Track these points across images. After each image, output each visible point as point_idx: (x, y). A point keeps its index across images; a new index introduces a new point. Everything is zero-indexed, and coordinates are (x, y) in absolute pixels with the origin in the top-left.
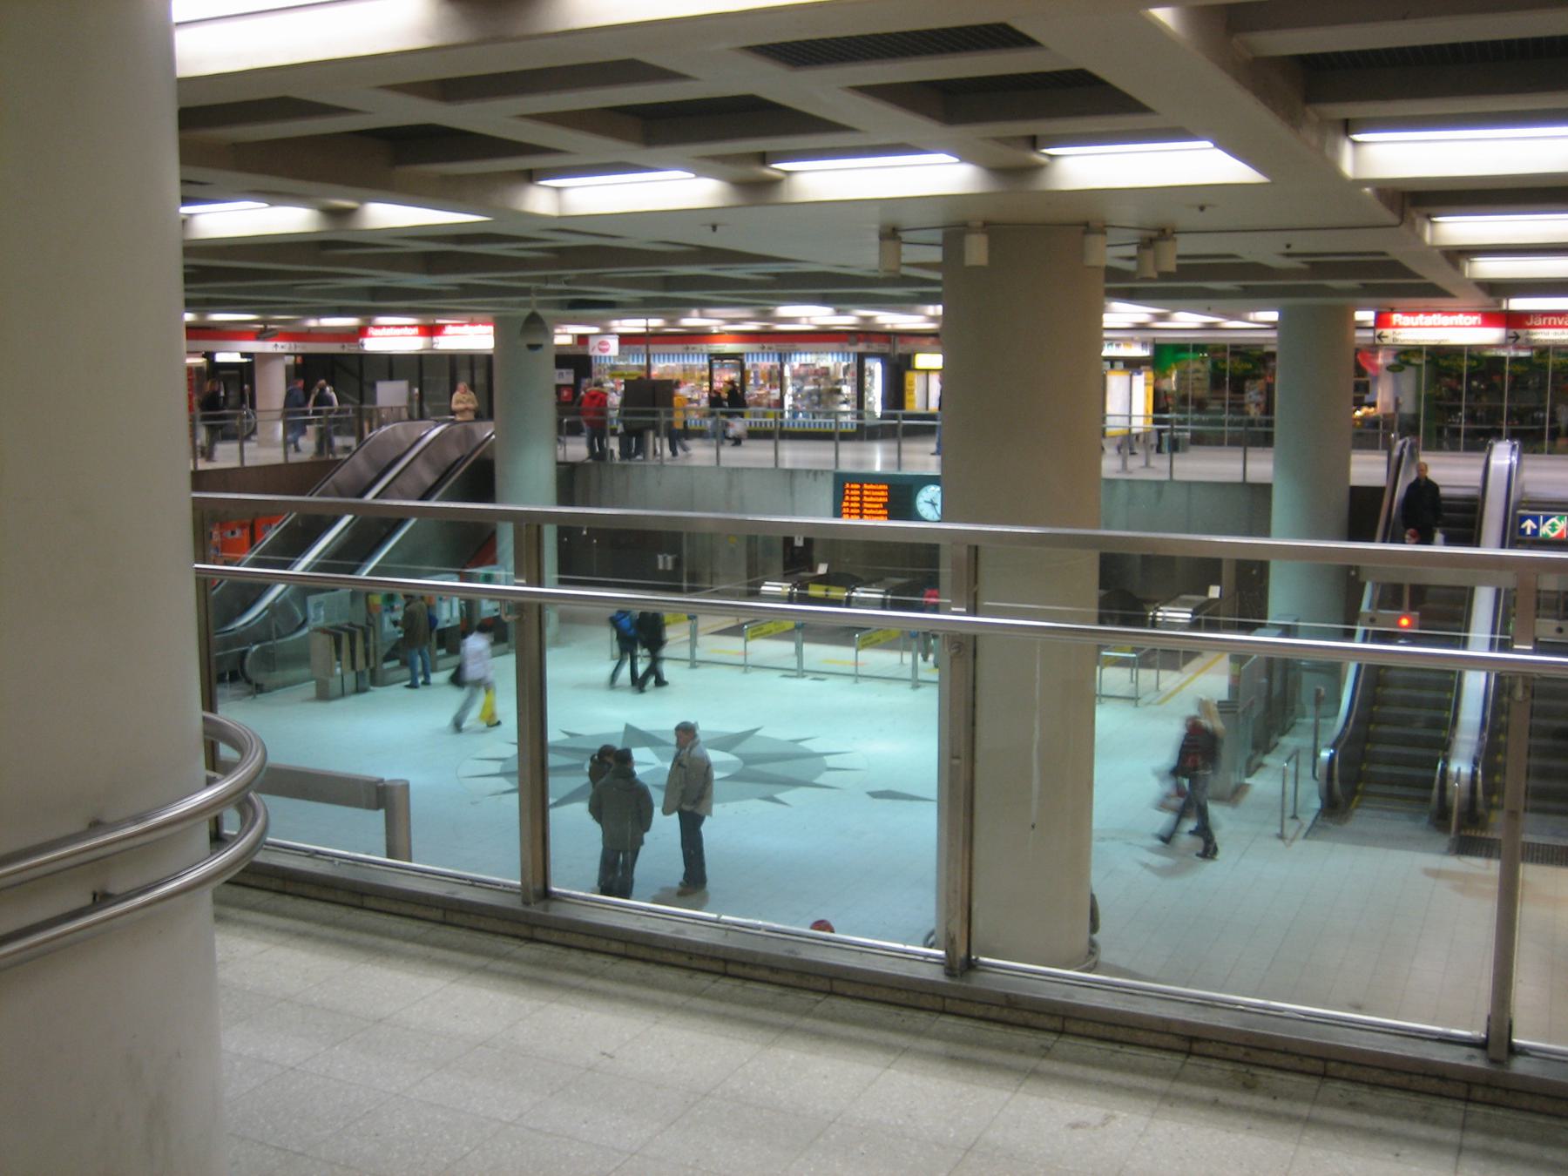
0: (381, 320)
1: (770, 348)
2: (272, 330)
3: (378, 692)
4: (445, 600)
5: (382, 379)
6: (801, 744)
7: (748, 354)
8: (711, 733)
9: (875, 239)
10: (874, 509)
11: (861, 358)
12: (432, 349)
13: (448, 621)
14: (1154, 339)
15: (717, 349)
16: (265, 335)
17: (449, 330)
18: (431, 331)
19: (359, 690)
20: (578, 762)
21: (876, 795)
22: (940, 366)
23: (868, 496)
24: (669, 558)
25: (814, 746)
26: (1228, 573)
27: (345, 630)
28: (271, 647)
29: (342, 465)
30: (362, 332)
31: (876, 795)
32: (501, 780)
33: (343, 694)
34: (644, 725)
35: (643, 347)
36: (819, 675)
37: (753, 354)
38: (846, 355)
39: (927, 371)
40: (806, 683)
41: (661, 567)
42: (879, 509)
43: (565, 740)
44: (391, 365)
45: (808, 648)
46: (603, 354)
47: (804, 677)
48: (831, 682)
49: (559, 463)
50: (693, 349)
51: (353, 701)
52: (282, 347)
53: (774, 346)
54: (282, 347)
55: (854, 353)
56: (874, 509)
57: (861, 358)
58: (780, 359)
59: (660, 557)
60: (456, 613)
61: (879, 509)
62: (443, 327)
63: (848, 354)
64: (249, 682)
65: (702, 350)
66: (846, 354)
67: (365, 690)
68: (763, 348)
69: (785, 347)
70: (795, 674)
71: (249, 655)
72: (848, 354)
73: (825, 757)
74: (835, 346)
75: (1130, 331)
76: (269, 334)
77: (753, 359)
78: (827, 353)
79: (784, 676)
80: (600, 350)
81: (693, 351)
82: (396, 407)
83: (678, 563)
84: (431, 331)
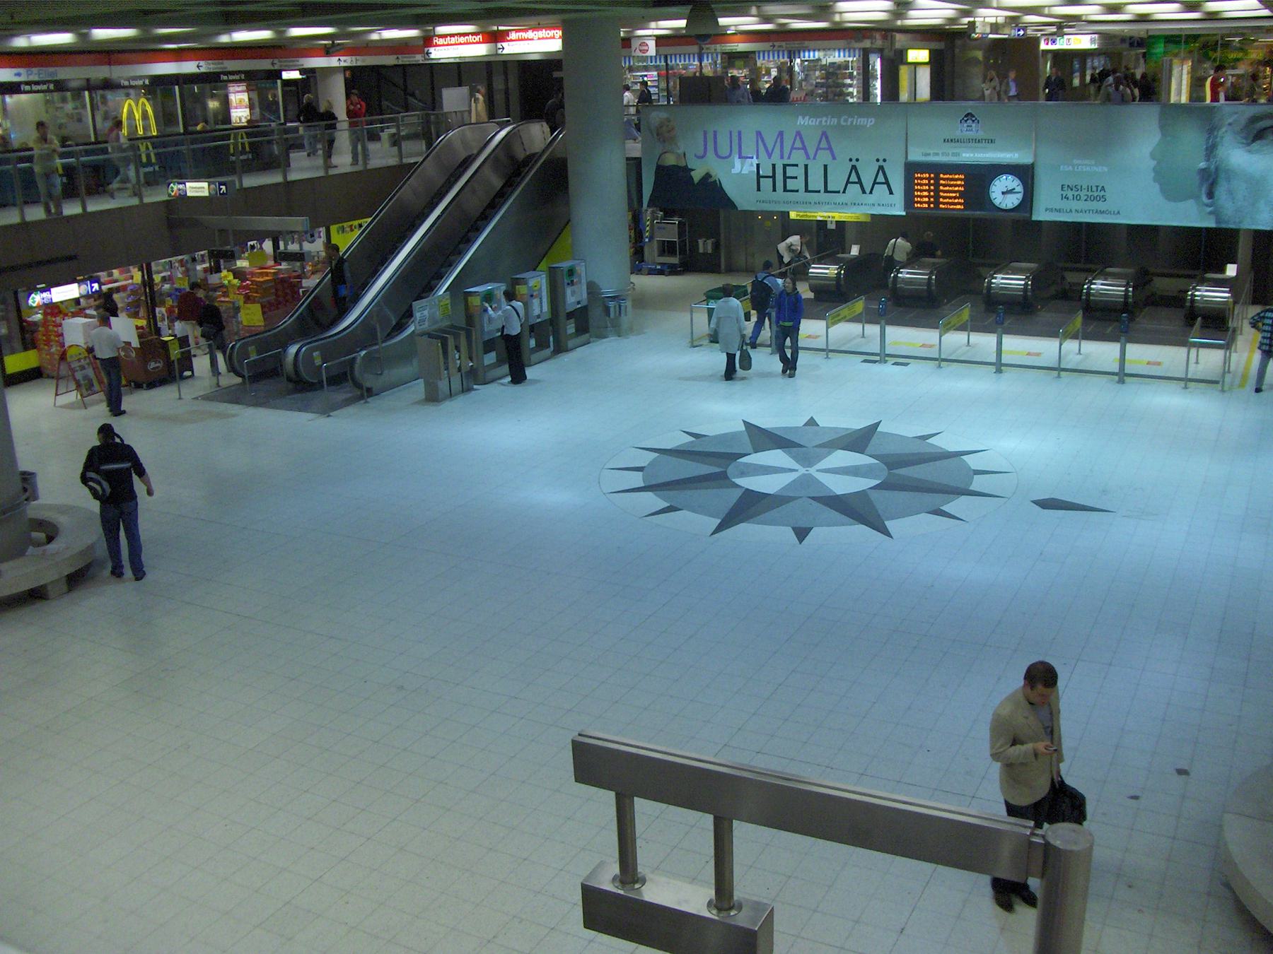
0: (442, 30)
1: (780, 46)
2: (339, 44)
3: (482, 391)
4: (536, 297)
5: (448, 86)
6: (930, 441)
7: (759, 52)
8: (835, 429)
9: (87, 77)
10: (950, 198)
11: (866, 54)
12: (497, 54)
13: (538, 317)
14: (1148, 30)
15: (729, 48)
16: (333, 49)
17: (513, 36)
18: (496, 38)
19: (466, 390)
20: (717, 470)
21: (1048, 504)
22: (927, 60)
23: (945, 186)
24: (710, 242)
25: (947, 442)
26: (1244, 248)
27: (448, 333)
28: (377, 351)
29: (418, 167)
30: (428, 41)
31: (1048, 504)
32: (649, 495)
33: (451, 395)
34: (766, 421)
35: (695, 49)
36: (902, 360)
37: (764, 52)
38: (852, 51)
39: (916, 65)
40: (888, 369)
41: (701, 250)
42: (955, 198)
43: (692, 442)
44: (460, 72)
45: (890, 330)
46: (644, 55)
47: (886, 362)
48: (914, 366)
49: (628, 159)
50: (707, 49)
51: (459, 402)
52: (345, 61)
53: (783, 44)
54: (345, 61)
55: (860, 49)
56: (950, 198)
57: (866, 54)
58: (789, 57)
59: (701, 242)
60: (546, 308)
61: (955, 198)
62: (507, 33)
63: (854, 50)
64: (358, 385)
65: (715, 50)
66: (850, 49)
67: (469, 390)
68: (774, 46)
69: (796, 44)
70: (878, 358)
71: (358, 361)
72: (854, 50)
73: (964, 457)
74: (841, 43)
75: (1132, 23)
76: (338, 48)
77: (676, 60)
78: (834, 49)
79: (865, 361)
80: (640, 51)
81: (709, 51)
82: (460, 112)
83: (717, 246)
84: (496, 38)
